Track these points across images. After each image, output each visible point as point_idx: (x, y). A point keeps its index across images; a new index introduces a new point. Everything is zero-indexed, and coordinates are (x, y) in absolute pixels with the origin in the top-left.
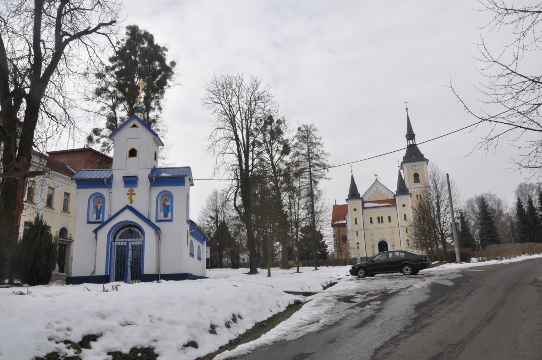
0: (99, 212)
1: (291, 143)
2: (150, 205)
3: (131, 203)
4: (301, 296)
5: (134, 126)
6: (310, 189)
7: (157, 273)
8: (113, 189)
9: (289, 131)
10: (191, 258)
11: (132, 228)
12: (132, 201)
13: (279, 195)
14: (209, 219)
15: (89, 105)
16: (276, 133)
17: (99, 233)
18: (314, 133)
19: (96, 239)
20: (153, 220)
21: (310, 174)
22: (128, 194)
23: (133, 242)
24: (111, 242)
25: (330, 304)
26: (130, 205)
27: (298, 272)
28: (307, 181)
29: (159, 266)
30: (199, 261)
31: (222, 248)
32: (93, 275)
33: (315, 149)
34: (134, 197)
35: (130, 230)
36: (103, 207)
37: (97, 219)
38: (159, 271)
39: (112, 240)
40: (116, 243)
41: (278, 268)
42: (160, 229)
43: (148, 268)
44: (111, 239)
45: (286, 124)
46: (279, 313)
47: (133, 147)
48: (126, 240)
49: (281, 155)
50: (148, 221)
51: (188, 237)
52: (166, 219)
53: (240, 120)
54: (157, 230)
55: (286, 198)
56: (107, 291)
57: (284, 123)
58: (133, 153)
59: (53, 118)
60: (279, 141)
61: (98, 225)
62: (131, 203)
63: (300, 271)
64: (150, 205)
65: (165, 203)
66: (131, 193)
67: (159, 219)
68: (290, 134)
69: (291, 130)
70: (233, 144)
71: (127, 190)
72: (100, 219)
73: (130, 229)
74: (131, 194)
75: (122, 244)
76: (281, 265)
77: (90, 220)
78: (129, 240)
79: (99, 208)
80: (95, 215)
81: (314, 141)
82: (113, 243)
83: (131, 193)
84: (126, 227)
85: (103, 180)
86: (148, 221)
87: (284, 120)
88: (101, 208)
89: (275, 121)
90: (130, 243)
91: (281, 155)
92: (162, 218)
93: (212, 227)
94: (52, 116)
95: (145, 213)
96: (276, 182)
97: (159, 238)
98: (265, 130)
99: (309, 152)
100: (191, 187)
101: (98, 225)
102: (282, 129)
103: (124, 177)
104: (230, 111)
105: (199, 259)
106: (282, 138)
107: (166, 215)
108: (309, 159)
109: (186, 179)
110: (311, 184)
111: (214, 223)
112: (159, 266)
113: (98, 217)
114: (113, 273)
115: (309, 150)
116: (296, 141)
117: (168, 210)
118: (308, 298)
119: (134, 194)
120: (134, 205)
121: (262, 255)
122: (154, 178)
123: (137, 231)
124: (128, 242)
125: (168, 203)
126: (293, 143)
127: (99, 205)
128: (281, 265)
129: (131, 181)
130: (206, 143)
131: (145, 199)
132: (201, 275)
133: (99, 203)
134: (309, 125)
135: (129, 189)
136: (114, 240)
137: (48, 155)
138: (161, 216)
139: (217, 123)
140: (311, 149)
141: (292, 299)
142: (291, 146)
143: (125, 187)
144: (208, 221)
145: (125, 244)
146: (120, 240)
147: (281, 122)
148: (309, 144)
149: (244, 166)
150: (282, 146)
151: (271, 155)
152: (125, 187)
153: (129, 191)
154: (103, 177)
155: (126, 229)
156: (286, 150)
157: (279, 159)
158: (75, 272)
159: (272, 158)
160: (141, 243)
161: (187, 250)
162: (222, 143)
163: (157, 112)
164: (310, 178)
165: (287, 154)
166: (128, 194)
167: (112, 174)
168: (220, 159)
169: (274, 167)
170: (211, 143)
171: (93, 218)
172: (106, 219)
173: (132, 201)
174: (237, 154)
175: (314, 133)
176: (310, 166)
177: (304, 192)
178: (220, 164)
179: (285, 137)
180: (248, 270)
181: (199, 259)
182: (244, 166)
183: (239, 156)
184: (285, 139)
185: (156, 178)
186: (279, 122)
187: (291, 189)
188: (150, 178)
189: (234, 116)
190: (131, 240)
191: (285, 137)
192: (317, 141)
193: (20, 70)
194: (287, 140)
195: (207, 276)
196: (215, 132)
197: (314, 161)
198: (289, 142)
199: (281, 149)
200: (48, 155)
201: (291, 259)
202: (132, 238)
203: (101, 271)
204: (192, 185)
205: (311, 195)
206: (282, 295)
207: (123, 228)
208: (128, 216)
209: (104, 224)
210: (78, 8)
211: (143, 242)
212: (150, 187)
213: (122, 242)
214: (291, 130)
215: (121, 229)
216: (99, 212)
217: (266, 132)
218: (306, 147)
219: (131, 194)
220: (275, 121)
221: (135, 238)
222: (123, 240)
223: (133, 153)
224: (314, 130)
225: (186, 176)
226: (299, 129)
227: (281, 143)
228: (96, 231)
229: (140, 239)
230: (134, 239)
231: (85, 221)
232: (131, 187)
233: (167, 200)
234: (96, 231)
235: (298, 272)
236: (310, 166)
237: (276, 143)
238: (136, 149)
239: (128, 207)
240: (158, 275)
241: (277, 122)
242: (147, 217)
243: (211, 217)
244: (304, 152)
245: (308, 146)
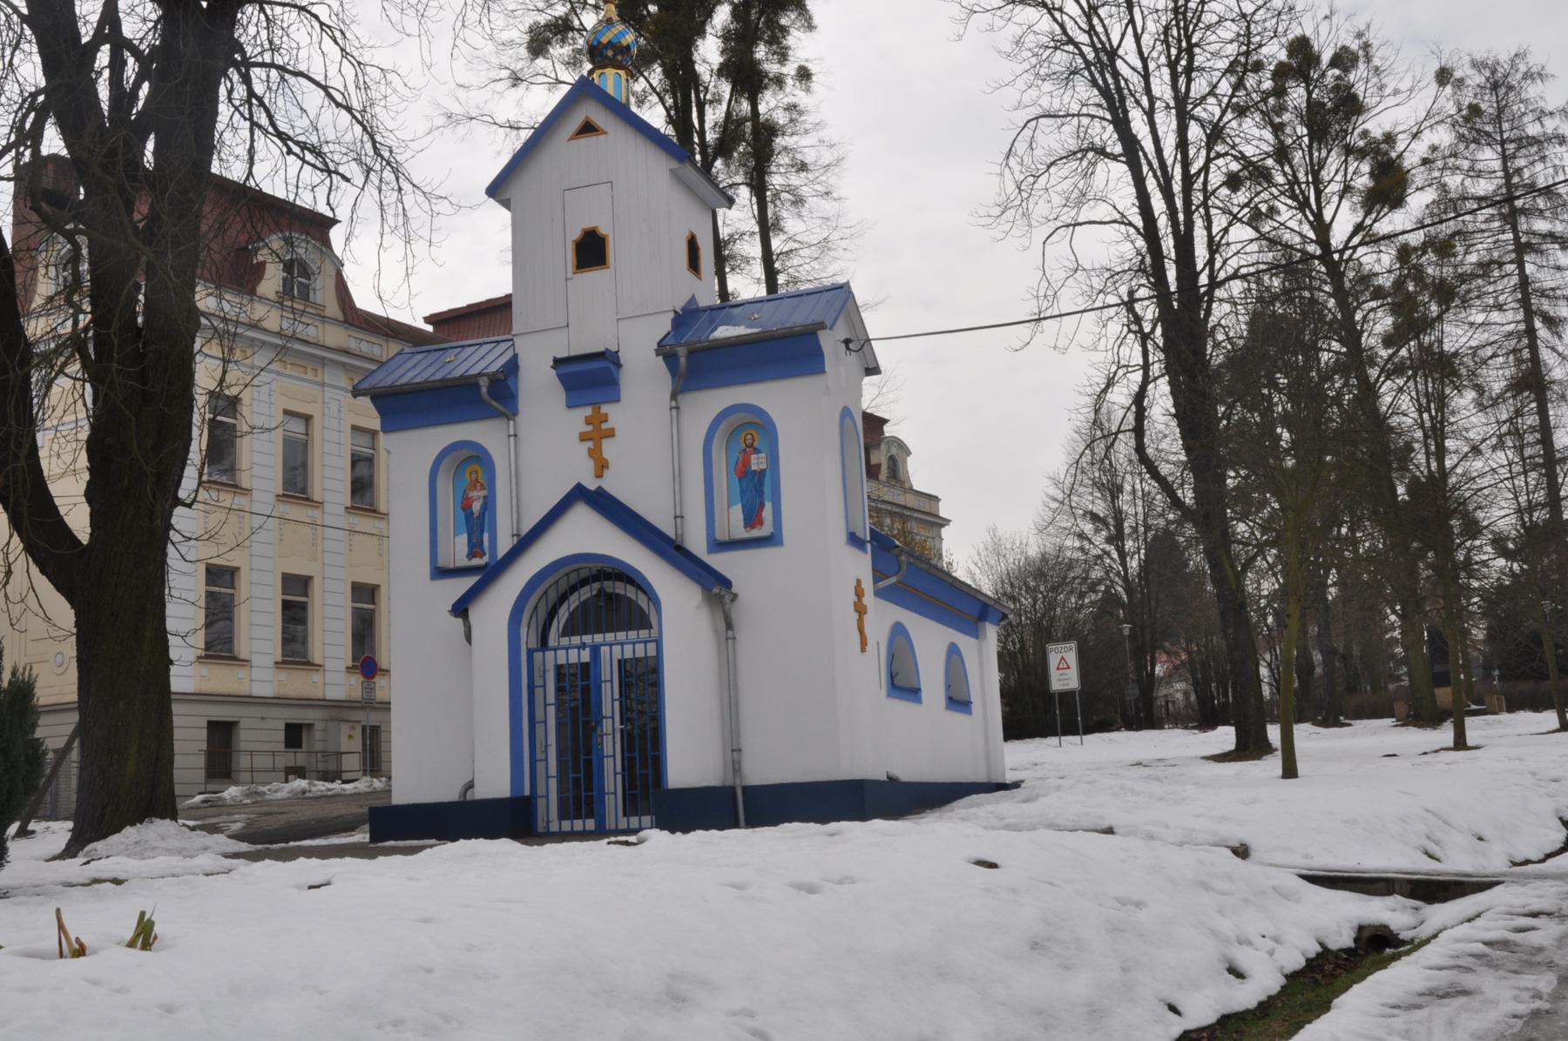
0: (477, 524)
1: (1412, 154)
2: (678, 477)
3: (599, 476)
4: (1397, 900)
5: (588, 129)
6: (1526, 354)
7: (729, 783)
8: (522, 418)
9: (1396, 92)
10: (901, 707)
11: (609, 586)
12: (601, 467)
13: (1369, 392)
14: (1088, 528)
15: (519, 103)
16: (1335, 110)
17: (477, 613)
18: (1532, 91)
19: (469, 638)
20: (697, 543)
21: (1524, 281)
22: (584, 437)
23: (616, 647)
24: (530, 652)
25: (1528, 980)
26: (591, 484)
27: (1460, 743)
28: (1509, 319)
29: (734, 753)
30: (957, 717)
31: (1115, 650)
32: (469, 797)
33: (1539, 167)
34: (609, 448)
35: (601, 598)
36: (489, 503)
37: (471, 555)
38: (736, 768)
39: (533, 644)
40: (550, 654)
41: (1389, 721)
42: (727, 583)
43: (689, 761)
44: (528, 638)
45: (1376, 62)
46: (1225, 1020)
47: (588, 225)
48: (587, 639)
49: (1367, 213)
50: (672, 551)
51: (860, 610)
52: (756, 533)
53: (1139, 65)
54: (715, 587)
55: (1405, 403)
56: (80, 951)
57: (1368, 59)
58: (591, 251)
59: (309, 157)
60: (1349, 150)
61: (468, 582)
62: (599, 476)
63: (1471, 737)
64: (678, 477)
65: (746, 462)
66: (597, 428)
67: (721, 535)
68: (1401, 110)
69: (1404, 86)
70: (1115, 178)
71: (577, 419)
72: (482, 554)
73: (601, 591)
74: (597, 434)
75: (573, 657)
76: (1400, 707)
77: (445, 561)
78: (599, 638)
79: (476, 506)
80: (462, 541)
81: (1533, 130)
82: (538, 656)
83: (597, 428)
84: (584, 582)
85: (477, 386)
86: (672, 551)
87: (1366, 46)
88: (485, 507)
89: (1326, 58)
90: (605, 650)
91: (1367, 213)
92: (740, 532)
93: (1099, 557)
94: (303, 146)
95: (658, 514)
96: (1351, 335)
97: (729, 625)
98: (1281, 109)
99: (1508, 184)
100: (867, 379)
101: (468, 582)
102: (1359, 89)
103: (558, 363)
104: (1091, 31)
105: (958, 702)
106: (1365, 134)
107: (753, 519)
108: (1511, 218)
109: (829, 342)
110: (1531, 332)
111: (1109, 540)
112: (734, 753)
113: (475, 549)
114: (550, 792)
115: (1508, 176)
116: (1443, 137)
117: (760, 493)
118: (1440, 913)
119: (611, 433)
120: (617, 485)
121: (1319, 671)
122: (682, 352)
123: (631, 592)
124: (595, 650)
125: (758, 462)
126: (1420, 149)
127: (475, 494)
128: (1400, 707)
129: (589, 377)
130: (991, 185)
131: (657, 449)
132: (981, 777)
133: (474, 484)
134: (1504, 57)
135: (588, 411)
136: (544, 644)
137: (430, 328)
138: (733, 522)
139: (1033, 93)
140: (1519, 171)
141: (1339, 917)
142: (1410, 161)
143: (570, 406)
144: (1081, 536)
145: (586, 656)
146: (565, 641)
147: (1354, 60)
148: (1511, 147)
149: (1171, 274)
150: (1365, 167)
151: (1319, 215)
152: (570, 406)
153: (588, 421)
154: (475, 371)
155: (586, 593)
156: (1388, 186)
157: (1358, 228)
158: (414, 779)
159: (1322, 229)
160: (652, 648)
161: (870, 670)
162: (1063, 179)
163: (792, 92)
164: (1525, 303)
165: (1397, 202)
166: (584, 437)
167: (515, 357)
168: (1059, 248)
169: (1335, 272)
170: (1011, 187)
171: (457, 550)
172: (504, 545)
173: (601, 467)
174: (1140, 224)
175: (1532, 91)
176: (1522, 249)
177: (1497, 377)
178: (1057, 275)
179: (1375, 124)
180: (1224, 737)
181: (958, 702)
182: (1171, 274)
183: (1150, 232)
184: (1377, 133)
185: (692, 353)
186: (1344, 59)
187: (1441, 369)
188: (665, 351)
189: (1113, 54)
190: (610, 637)
191: (1375, 124)
192: (1550, 125)
193: (1373, 373)
194: (1390, 138)
195: (1010, 777)
196: (1027, 133)
197: (1541, 225)
198: (1400, 146)
199: (1363, 182)
200: (430, 328)
201: (1442, 680)
202: (599, 631)
203: (495, 783)
204: (873, 370)
205: (1531, 381)
206: (1286, 895)
207: (573, 589)
208: (586, 535)
209: (490, 574)
210: (1056, 48)
211: (659, 643)
212: (674, 396)
213: (575, 654)
214: (1404, 86)
215: (563, 598)
216: (477, 524)
217: (1286, 117)
218: (1497, 165)
219: (597, 434)
220: (1326, 58)
221: (629, 627)
222: (576, 640)
223: (591, 251)
224: (1528, 76)
225: (822, 326)
226: (1443, 76)
227: (1361, 154)
228: (461, 609)
229: (644, 633)
230: (621, 636)
231: (426, 569)
232: (596, 405)
233: (752, 448)
234: (461, 609)
235: (1460, 743)
236: (1522, 249)
237: (1334, 161)
238: (603, 230)
239: (579, 494)
240: (732, 789)
241: (1334, 62)
242: (668, 529)
243: (1094, 517)
244: (1484, 187)
245: (1505, 158)
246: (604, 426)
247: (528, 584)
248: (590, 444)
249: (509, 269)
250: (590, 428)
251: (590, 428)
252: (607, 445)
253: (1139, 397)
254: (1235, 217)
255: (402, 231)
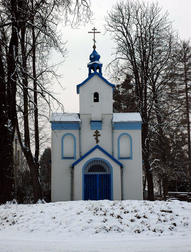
3: (97, 143)
12: (97, 141)
22: (94, 135)
62: (97, 143)
74: (97, 135)
77: (65, 155)
83: (97, 134)
119: (100, 135)
166: (94, 135)
173: (97, 141)
208: (97, 154)
219: (97, 135)
231: (60, 157)
246: (98, 134)
247: (75, 138)
248: (95, 137)
249: (99, 145)
250: (95, 134)
251: (95, 134)
252: (99, 137)
253: (170, 199)
254: (158, 31)
255: (138, 24)
